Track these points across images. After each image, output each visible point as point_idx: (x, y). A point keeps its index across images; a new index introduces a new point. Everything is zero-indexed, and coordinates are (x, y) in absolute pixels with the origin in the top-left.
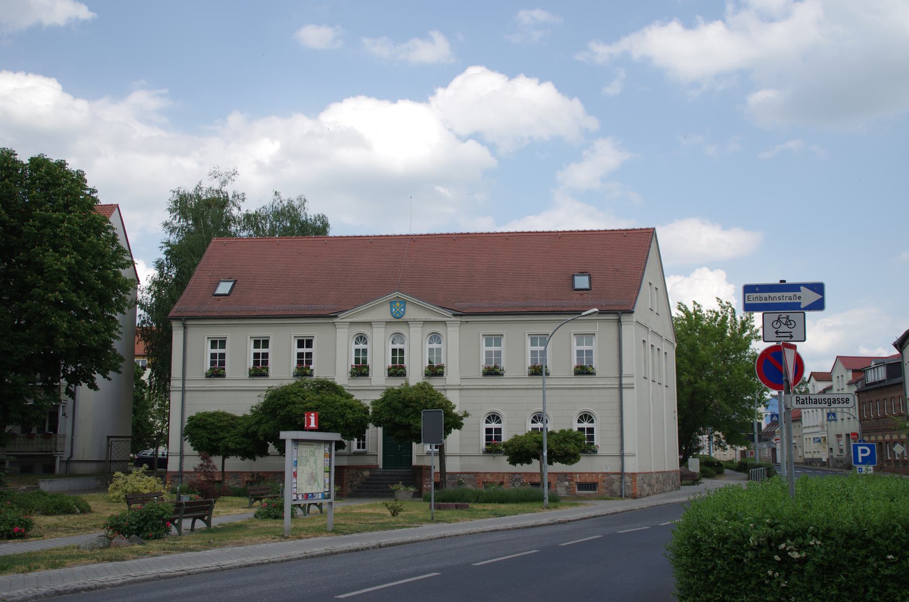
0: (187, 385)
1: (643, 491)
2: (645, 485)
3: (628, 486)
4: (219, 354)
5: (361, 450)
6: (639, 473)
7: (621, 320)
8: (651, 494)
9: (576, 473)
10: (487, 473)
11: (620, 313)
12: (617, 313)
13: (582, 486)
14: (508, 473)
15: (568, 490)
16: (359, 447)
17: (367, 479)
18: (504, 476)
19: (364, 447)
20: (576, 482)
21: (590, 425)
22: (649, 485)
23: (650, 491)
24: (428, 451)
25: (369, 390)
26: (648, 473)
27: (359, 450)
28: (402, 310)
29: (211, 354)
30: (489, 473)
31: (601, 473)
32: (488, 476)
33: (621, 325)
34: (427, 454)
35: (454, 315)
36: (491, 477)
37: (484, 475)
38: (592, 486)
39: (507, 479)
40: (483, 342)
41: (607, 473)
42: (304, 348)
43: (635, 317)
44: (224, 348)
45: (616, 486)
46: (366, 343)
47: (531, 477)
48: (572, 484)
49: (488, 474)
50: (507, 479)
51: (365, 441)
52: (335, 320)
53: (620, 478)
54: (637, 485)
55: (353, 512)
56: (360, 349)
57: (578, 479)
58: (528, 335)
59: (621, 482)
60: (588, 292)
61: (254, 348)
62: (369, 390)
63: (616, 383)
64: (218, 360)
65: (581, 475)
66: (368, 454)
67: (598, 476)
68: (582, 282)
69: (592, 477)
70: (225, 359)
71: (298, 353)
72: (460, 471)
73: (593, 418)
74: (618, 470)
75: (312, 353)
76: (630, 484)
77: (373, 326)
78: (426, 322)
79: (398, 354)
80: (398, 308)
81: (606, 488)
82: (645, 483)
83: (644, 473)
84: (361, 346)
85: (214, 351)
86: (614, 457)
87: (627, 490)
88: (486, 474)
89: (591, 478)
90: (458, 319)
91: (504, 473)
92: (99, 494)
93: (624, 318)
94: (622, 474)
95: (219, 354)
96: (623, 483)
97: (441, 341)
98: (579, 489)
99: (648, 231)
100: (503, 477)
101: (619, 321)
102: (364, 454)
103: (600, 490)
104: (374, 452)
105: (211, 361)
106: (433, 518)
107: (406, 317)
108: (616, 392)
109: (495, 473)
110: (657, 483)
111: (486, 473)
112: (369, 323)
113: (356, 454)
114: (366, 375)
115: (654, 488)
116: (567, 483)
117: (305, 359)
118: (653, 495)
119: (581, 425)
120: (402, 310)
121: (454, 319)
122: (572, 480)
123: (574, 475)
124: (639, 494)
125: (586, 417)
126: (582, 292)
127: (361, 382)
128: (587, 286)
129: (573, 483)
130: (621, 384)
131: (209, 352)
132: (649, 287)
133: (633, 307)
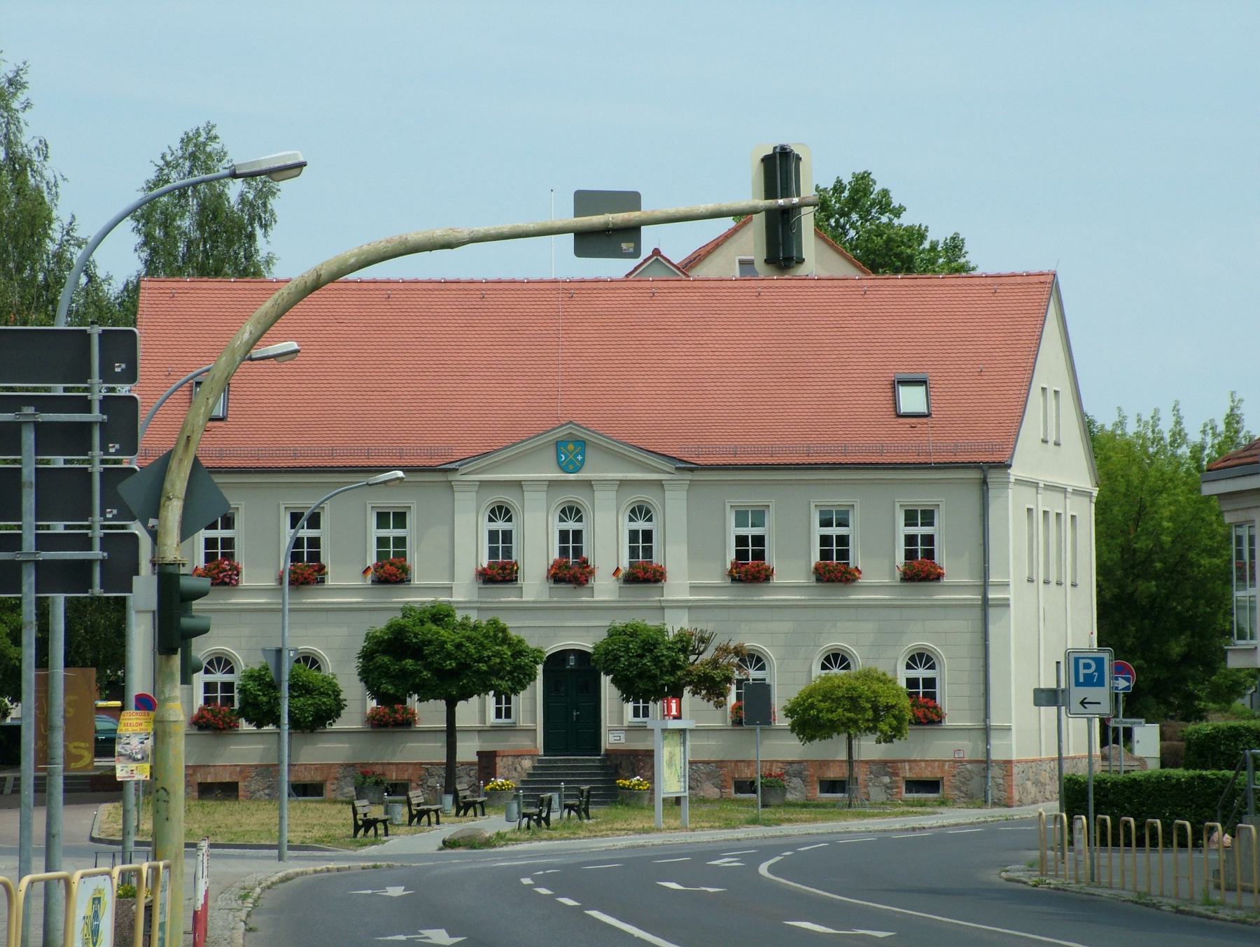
1: (1025, 794)
2: (1029, 784)
3: (998, 785)
4: (643, 531)
5: (503, 721)
6: (1019, 762)
7: (988, 480)
8: (1040, 799)
9: (904, 761)
11: (985, 468)
12: (980, 468)
13: (916, 785)
15: (888, 791)
16: (498, 715)
17: (530, 775)
18: (771, 766)
19: (508, 715)
20: (903, 778)
21: (929, 674)
22: (1036, 783)
23: (1038, 795)
26: (1033, 761)
27: (499, 721)
28: (580, 458)
31: (948, 761)
33: (988, 489)
35: (678, 469)
37: (736, 765)
38: (932, 786)
40: (731, 519)
43: (1014, 473)
44: (931, 524)
45: (976, 783)
46: (510, 520)
47: (821, 768)
48: (896, 782)
49: (742, 764)
51: (497, 708)
52: (451, 477)
53: (984, 769)
54: (1014, 783)
56: (837, 526)
57: (908, 771)
58: (901, 506)
59: (986, 777)
60: (924, 420)
61: (906, 525)
63: (974, 597)
64: (305, 550)
65: (913, 765)
66: (518, 728)
67: (943, 766)
68: (913, 400)
69: (933, 768)
73: (935, 660)
74: (981, 757)
75: (821, 526)
76: (1001, 781)
77: (595, 488)
78: (623, 483)
79: (571, 541)
80: (571, 453)
81: (959, 789)
82: (1029, 780)
83: (1027, 762)
84: (500, 525)
85: (384, 533)
86: (973, 732)
87: (996, 792)
88: (739, 764)
89: (930, 769)
90: (688, 476)
91: (772, 762)
93: (993, 476)
94: (986, 763)
95: (643, 531)
96: (990, 779)
97: (581, 516)
98: (909, 790)
99: (1042, 279)
101: (984, 482)
102: (512, 729)
103: (946, 790)
104: (530, 725)
105: (206, 553)
106: (736, 765)
108: (977, 613)
110: (1051, 779)
111: (737, 761)
112: (518, 484)
113: (495, 729)
115: (1045, 789)
116: (887, 780)
118: (1043, 802)
119: (913, 674)
120: (580, 458)
121: (677, 476)
122: (896, 774)
123: (899, 765)
124: (1017, 798)
125: (920, 658)
126: (914, 420)
128: (904, 391)
129: (897, 778)
130: (985, 600)
132: (1041, 399)
133: (1012, 456)
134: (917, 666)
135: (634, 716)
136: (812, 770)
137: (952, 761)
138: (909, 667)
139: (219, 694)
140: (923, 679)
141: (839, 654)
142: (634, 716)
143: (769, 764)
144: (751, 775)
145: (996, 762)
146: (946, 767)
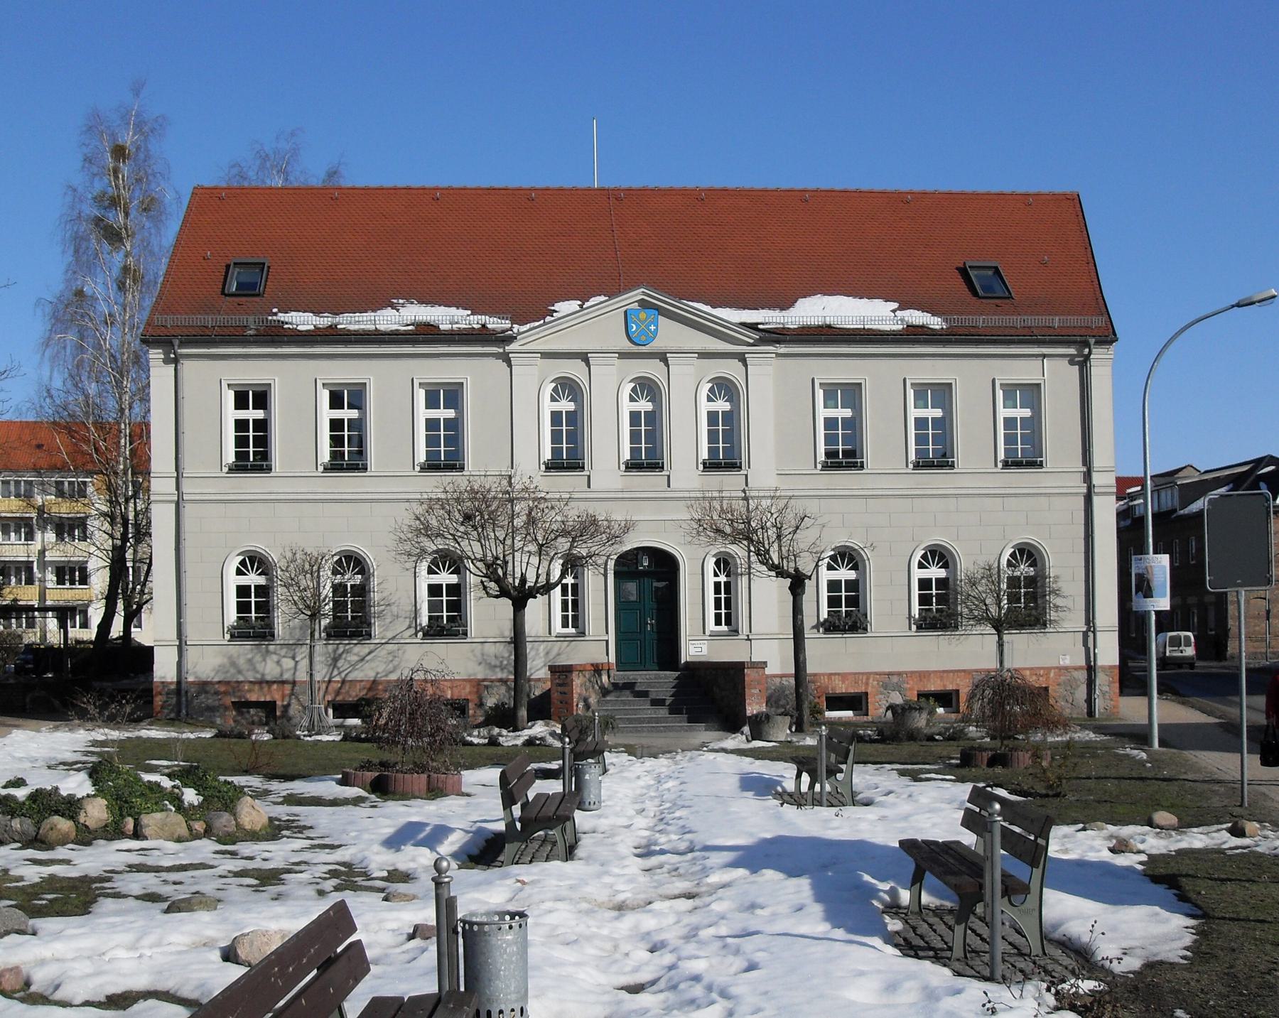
0: (186, 488)
10: (835, 674)
14: (876, 674)
18: (868, 679)
24: (711, 631)
25: (308, 501)
27: (566, 631)
28: (652, 328)
29: (237, 421)
30: (839, 674)
32: (837, 682)
34: (710, 636)
36: (843, 682)
39: (873, 687)
41: (1066, 668)
42: (248, 408)
47: (921, 680)
50: (873, 687)
55: (1108, 738)
60: (1007, 301)
61: (236, 408)
62: (308, 501)
70: (552, 430)
71: (426, 419)
72: (779, 672)
78: (704, 355)
88: (833, 677)
91: (868, 674)
92: (38, 731)
100: (867, 684)
107: (657, 345)
109: (850, 674)
111: (831, 674)
114: (579, 467)
117: (930, 432)
120: (652, 328)
127: (566, 482)
130: (1090, 488)
131: (421, 415)
134: (929, 564)
135: (716, 625)
136: (911, 682)
137: (1057, 668)
138: (239, 572)
139: (934, 592)
140: (447, 585)
141: (936, 551)
142: (716, 625)
143: (865, 677)
144: (846, 689)
145: (1103, 668)
146: (1052, 675)
